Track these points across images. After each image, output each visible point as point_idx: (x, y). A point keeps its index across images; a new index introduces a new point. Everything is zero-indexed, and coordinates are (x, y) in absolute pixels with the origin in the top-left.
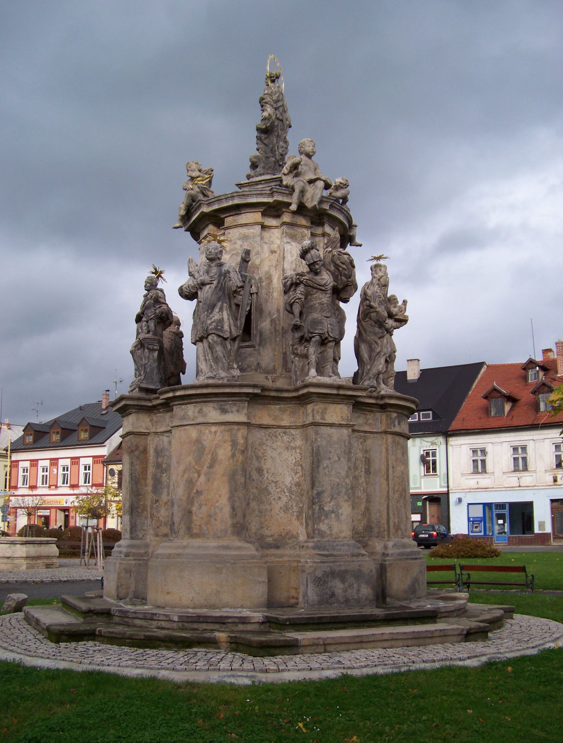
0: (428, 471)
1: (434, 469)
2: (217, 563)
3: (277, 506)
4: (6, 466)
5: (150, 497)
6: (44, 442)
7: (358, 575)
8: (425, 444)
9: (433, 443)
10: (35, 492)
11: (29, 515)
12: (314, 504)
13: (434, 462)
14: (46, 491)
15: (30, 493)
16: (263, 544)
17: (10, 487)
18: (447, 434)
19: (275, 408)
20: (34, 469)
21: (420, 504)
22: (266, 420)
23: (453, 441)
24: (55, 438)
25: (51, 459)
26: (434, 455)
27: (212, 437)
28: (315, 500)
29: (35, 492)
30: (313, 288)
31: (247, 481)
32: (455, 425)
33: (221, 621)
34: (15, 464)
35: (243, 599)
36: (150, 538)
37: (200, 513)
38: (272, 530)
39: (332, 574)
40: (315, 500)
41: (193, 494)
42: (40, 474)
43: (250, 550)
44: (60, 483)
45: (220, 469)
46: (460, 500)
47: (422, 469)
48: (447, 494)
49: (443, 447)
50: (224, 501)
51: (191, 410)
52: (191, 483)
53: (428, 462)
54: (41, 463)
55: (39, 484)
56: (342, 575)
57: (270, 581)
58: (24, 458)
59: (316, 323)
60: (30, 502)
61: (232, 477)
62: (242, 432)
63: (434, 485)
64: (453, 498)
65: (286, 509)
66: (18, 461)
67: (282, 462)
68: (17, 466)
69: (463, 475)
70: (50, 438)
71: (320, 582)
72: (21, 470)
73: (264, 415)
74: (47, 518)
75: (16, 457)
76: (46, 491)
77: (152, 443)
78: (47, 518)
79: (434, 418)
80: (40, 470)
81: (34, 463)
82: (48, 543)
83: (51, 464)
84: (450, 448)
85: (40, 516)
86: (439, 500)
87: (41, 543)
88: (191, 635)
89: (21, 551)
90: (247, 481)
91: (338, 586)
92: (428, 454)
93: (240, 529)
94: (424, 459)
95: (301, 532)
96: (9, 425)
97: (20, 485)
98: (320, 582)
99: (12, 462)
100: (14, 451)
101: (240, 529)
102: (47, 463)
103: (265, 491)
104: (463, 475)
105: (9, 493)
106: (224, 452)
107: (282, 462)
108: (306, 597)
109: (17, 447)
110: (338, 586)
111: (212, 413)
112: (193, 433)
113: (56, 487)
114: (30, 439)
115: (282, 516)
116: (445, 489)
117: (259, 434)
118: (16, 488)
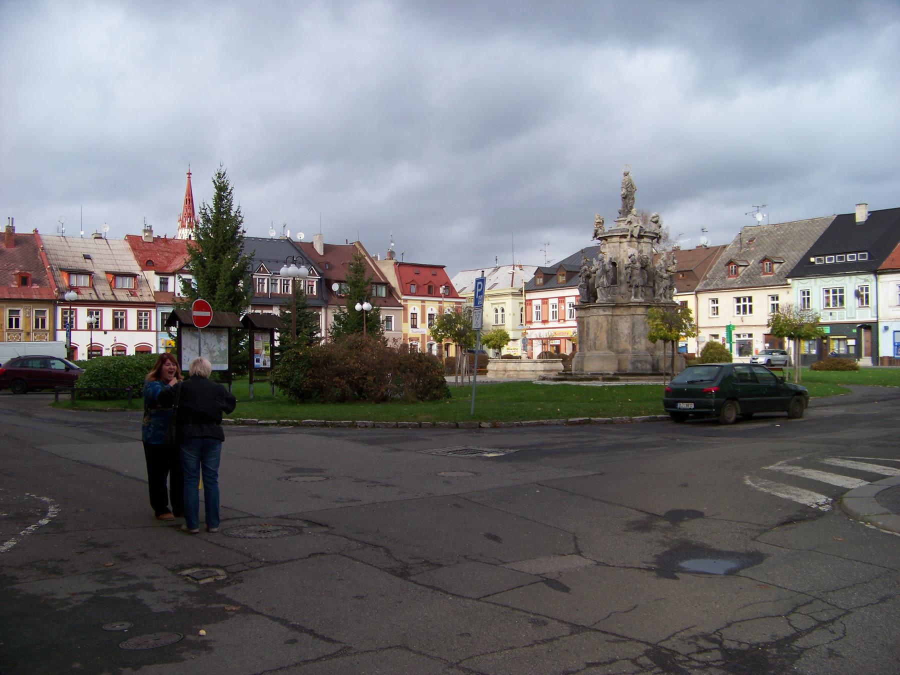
0: (862, 303)
1: (867, 302)
2: (603, 358)
3: (623, 340)
4: (521, 303)
5: (585, 338)
6: (552, 282)
7: (646, 362)
8: (859, 280)
9: (866, 280)
10: (547, 326)
11: (544, 344)
12: (633, 339)
13: (867, 296)
14: (556, 325)
15: (543, 326)
16: (618, 352)
17: (527, 322)
18: (877, 272)
19: (622, 309)
20: (545, 306)
21: (855, 331)
22: (619, 313)
23: (883, 278)
24: (562, 279)
25: (559, 298)
26: (867, 290)
27: (601, 319)
28: (634, 338)
29: (547, 326)
30: (633, 268)
31: (612, 333)
32: (885, 265)
33: (602, 374)
34: (529, 302)
35: (610, 368)
36: (586, 351)
37: (598, 343)
38: (621, 348)
39: (637, 361)
40: (634, 338)
41: (596, 337)
42: (551, 310)
43: (613, 354)
44: (567, 318)
45: (604, 329)
46: (886, 328)
47: (857, 302)
48: (877, 323)
49: (874, 283)
50: (605, 339)
51: (595, 310)
52: (595, 334)
53: (862, 296)
54: (551, 301)
55: (550, 318)
56: (640, 362)
57: (619, 364)
58: (536, 297)
59: (634, 281)
60: (544, 334)
61: (607, 332)
62: (610, 318)
63: (865, 316)
64: (881, 327)
65: (626, 341)
66: (531, 300)
67: (624, 326)
68: (531, 304)
69: (890, 307)
70: (557, 279)
71: (633, 363)
72: (534, 308)
73: (618, 312)
74: (558, 347)
75: (529, 296)
76: (556, 325)
77: (585, 320)
78: (558, 347)
79: (869, 258)
80: (550, 307)
81: (545, 301)
82: (556, 362)
83: (559, 302)
84: (880, 285)
85: (553, 346)
86: (870, 327)
87: (552, 362)
88: (593, 377)
89: (540, 367)
90: (612, 333)
91: (639, 365)
92: (862, 289)
93: (610, 347)
94: (858, 294)
95: (630, 348)
96: (520, 266)
97: (534, 320)
98: (633, 363)
99: (526, 301)
100: (527, 291)
101: (610, 347)
102: (556, 301)
103: (618, 336)
104: (890, 307)
105: (525, 327)
106: (605, 324)
107: (624, 326)
108: (629, 368)
109: (531, 287)
110: (639, 365)
111: (601, 312)
112: (596, 318)
113: (565, 320)
114: (540, 281)
115: (624, 343)
116: (875, 319)
117: (616, 318)
118: (531, 322)
